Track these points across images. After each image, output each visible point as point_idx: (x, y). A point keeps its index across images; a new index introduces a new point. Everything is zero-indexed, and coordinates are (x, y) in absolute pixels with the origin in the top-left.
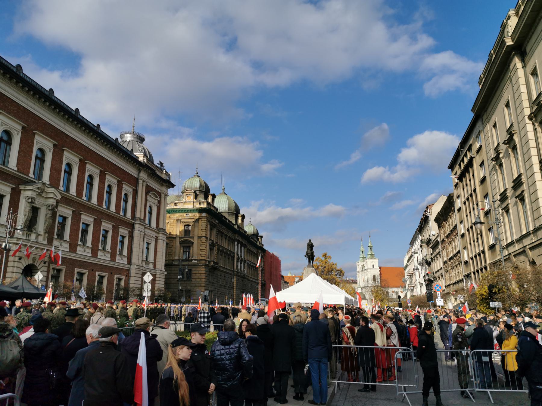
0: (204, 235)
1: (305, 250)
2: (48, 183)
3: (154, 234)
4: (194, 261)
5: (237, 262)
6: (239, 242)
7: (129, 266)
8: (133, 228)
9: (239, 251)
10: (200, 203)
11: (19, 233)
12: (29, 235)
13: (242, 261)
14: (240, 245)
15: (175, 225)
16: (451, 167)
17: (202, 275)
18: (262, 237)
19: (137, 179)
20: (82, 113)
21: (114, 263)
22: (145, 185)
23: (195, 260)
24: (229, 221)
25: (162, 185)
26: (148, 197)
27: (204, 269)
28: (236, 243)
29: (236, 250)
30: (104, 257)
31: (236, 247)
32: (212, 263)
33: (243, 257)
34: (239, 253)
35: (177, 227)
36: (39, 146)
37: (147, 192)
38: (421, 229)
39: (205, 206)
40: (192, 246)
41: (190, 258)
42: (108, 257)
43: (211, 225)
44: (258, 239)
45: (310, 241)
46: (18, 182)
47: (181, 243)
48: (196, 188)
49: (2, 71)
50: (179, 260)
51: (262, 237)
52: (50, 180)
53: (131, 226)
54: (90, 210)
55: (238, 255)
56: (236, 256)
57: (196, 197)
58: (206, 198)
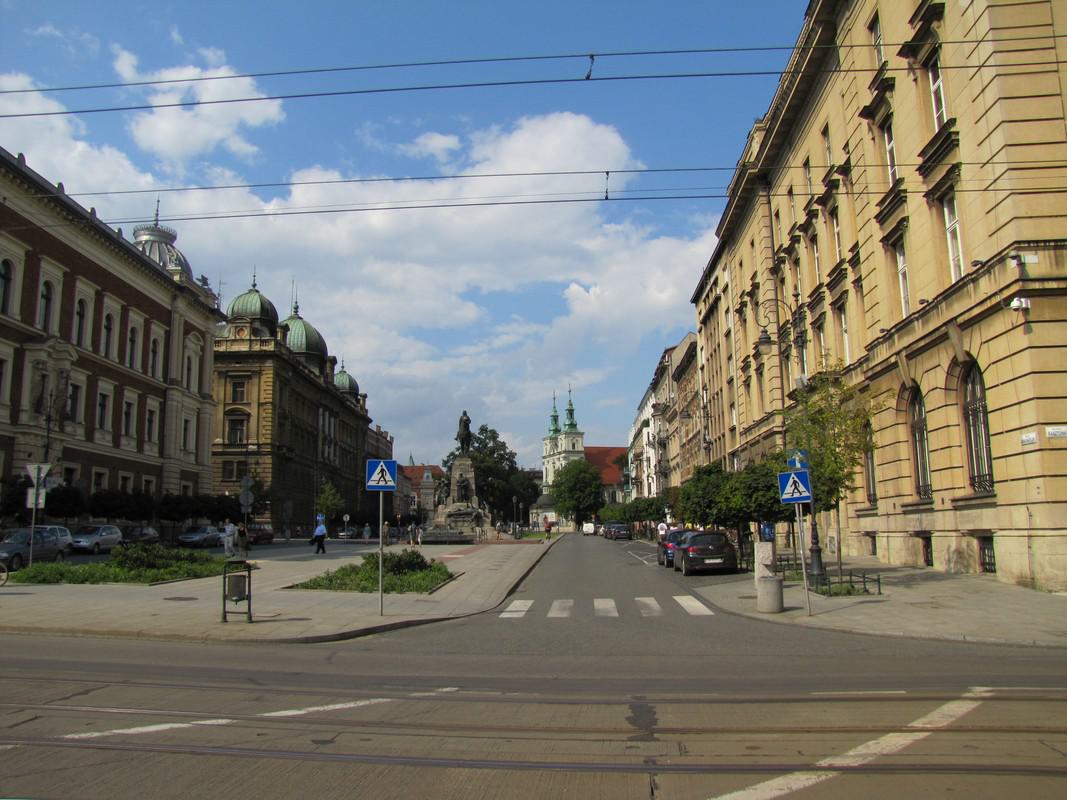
0: (271, 400)
1: (456, 428)
2: (58, 334)
3: (194, 404)
4: (250, 447)
5: (323, 444)
6: (326, 408)
7: (162, 460)
8: (165, 398)
9: (327, 424)
10: (263, 342)
11: (24, 418)
12: (37, 419)
13: (330, 442)
14: (327, 413)
15: (216, 381)
16: (696, 300)
17: (267, 470)
18: (365, 396)
19: (170, 312)
20: (99, 216)
21: (90, 445)
22: (182, 322)
23: (253, 445)
24: (309, 371)
25: (207, 319)
26: (187, 340)
27: (270, 461)
28: (321, 410)
29: (321, 422)
30: (128, 446)
31: (321, 418)
32: (284, 450)
33: (332, 435)
34: (327, 430)
35: (218, 386)
36: (133, 325)
37: (186, 333)
38: (655, 386)
39: (271, 347)
40: (248, 421)
41: (245, 442)
42: (108, 442)
43: (281, 381)
44: (358, 401)
45: (465, 413)
46: (24, 339)
47: (226, 413)
48: (255, 314)
49: (3, 171)
50: (224, 445)
51: (365, 396)
52: (60, 331)
53: (163, 394)
54: (134, 382)
55: (324, 432)
56: (321, 435)
57: (255, 332)
58: (273, 333)
